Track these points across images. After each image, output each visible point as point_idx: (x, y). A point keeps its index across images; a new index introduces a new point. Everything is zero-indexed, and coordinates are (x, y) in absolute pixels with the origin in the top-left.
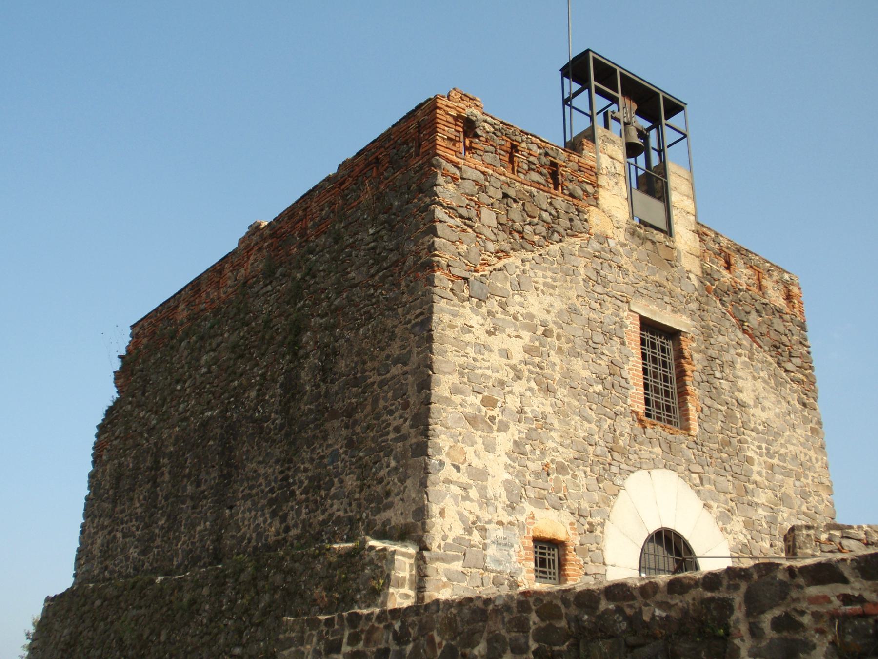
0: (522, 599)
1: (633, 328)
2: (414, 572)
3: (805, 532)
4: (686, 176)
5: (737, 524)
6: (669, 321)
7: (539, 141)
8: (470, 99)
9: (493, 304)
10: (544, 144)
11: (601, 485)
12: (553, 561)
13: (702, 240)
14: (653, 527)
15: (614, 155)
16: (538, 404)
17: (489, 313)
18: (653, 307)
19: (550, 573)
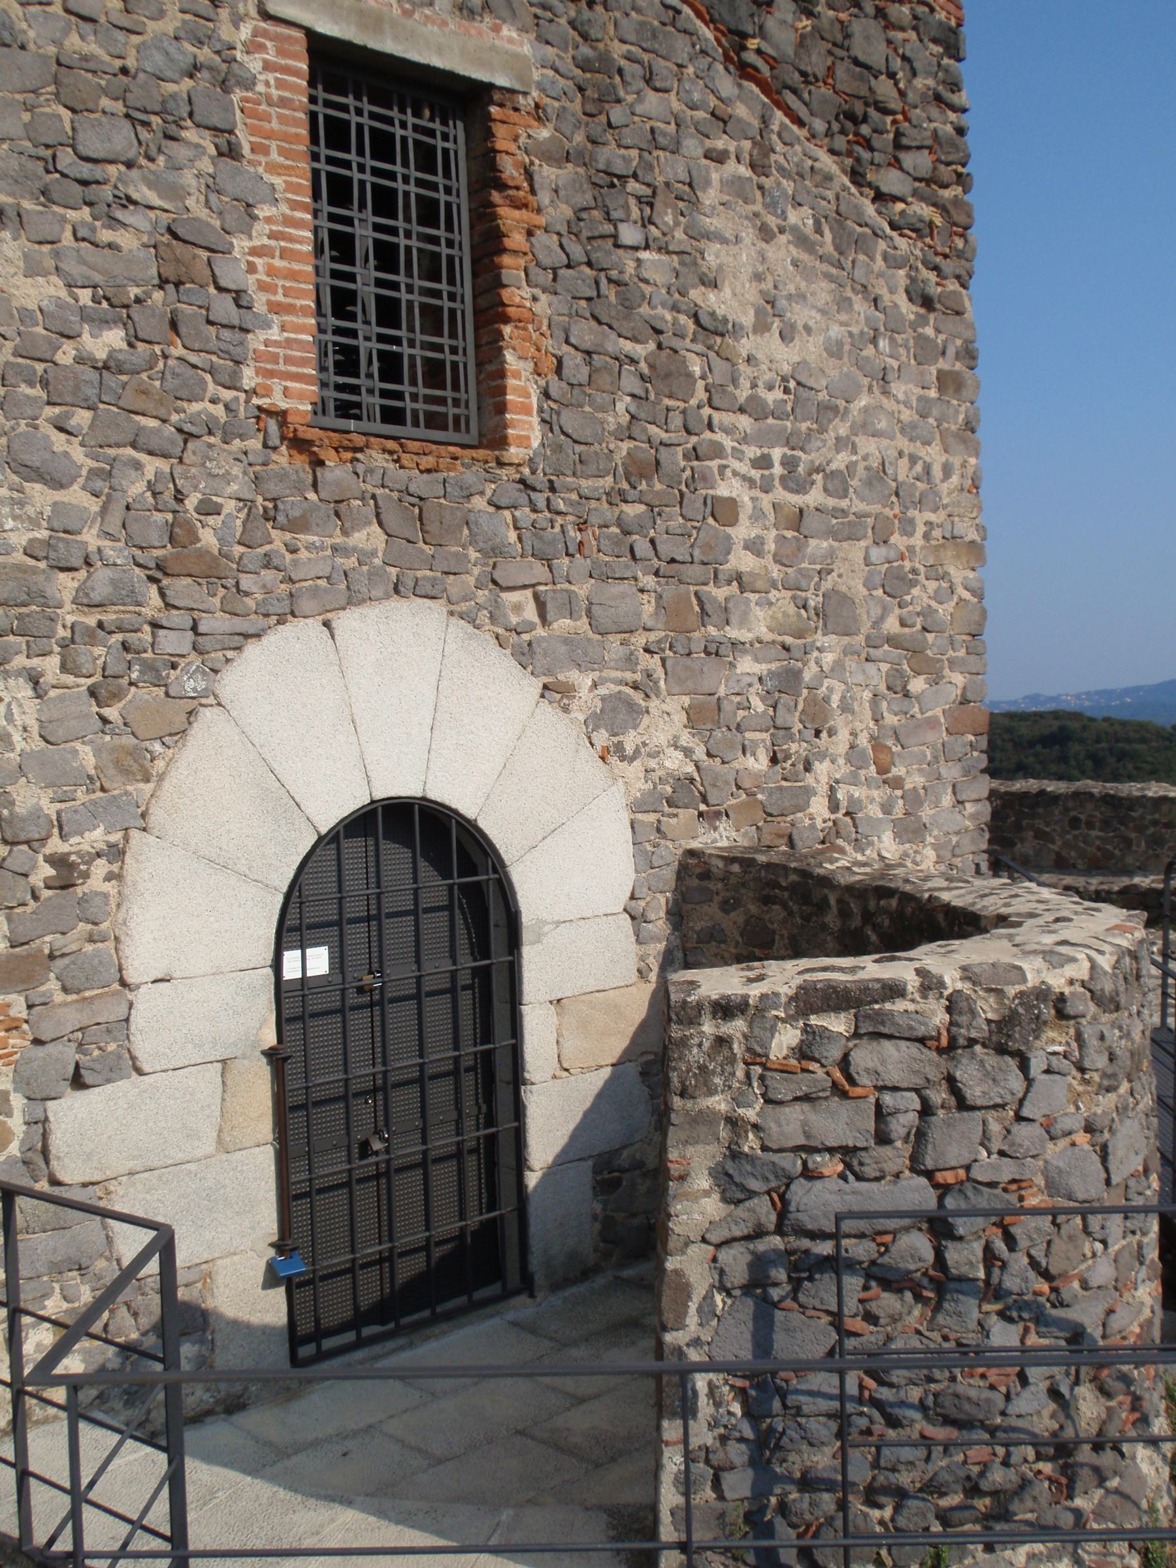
3: (708, 1027)
5: (664, 726)
6: (440, 51)
11: (112, 713)
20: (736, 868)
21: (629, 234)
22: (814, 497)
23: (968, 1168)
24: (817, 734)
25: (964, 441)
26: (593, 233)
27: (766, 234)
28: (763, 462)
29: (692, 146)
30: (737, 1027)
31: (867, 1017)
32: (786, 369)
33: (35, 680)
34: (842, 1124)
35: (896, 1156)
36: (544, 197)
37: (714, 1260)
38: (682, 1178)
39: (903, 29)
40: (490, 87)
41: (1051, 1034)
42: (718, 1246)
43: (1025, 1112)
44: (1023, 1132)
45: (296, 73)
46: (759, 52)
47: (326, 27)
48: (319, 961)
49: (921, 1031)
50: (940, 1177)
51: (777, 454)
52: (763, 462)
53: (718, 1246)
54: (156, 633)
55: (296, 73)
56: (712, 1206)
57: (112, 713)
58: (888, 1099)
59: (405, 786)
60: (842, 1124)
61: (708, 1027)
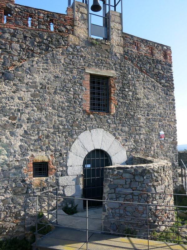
0: (133, 157)
1: (87, 79)
2: (181, 152)
3: (108, 171)
4: (134, 245)
5: (131, 143)
6: (104, 74)
7: (44, 12)
8: (11, 2)
9: (17, 81)
10: (46, 13)
11: (67, 139)
12: (45, 168)
13: (124, 39)
14: (91, 149)
15: (83, 12)
16: (37, 115)
17: (14, 85)
18: (97, 69)
19: (37, 173)
20: (138, 158)
21: (127, 90)
22: (151, 117)
23: (136, 188)
24: (152, 144)
25: (173, 110)
26: (122, 90)
27: (144, 88)
28: (144, 113)
29: (135, 80)
30: (111, 171)
31: (124, 171)
32: (147, 103)
33: (59, 136)
34: (122, 182)
35: (128, 186)
36: (116, 87)
37: (108, 195)
38: (105, 186)
39: (164, 65)
40: (110, 76)
41: (148, 174)
42: (108, 194)
43: (144, 182)
44: (143, 185)
45: (89, 77)
46: (144, 69)
47: (92, 73)
48: (89, 166)
49: (131, 173)
50: (133, 189)
51: (146, 112)
52: (144, 113)
53: (108, 194)
54: (71, 133)
55: (89, 77)
56: (108, 189)
57: (67, 139)
58: (127, 180)
59: (105, 149)
60: (122, 182)
61: (108, 171)
